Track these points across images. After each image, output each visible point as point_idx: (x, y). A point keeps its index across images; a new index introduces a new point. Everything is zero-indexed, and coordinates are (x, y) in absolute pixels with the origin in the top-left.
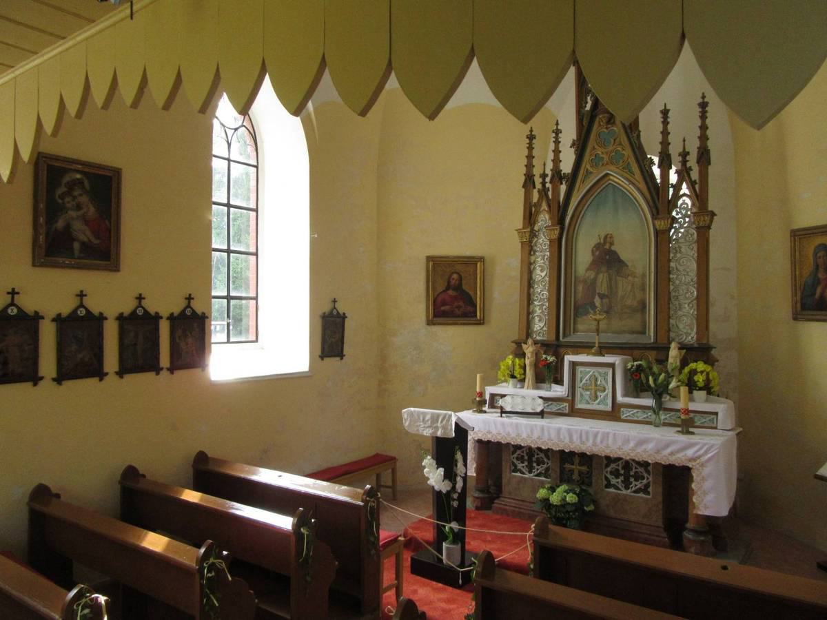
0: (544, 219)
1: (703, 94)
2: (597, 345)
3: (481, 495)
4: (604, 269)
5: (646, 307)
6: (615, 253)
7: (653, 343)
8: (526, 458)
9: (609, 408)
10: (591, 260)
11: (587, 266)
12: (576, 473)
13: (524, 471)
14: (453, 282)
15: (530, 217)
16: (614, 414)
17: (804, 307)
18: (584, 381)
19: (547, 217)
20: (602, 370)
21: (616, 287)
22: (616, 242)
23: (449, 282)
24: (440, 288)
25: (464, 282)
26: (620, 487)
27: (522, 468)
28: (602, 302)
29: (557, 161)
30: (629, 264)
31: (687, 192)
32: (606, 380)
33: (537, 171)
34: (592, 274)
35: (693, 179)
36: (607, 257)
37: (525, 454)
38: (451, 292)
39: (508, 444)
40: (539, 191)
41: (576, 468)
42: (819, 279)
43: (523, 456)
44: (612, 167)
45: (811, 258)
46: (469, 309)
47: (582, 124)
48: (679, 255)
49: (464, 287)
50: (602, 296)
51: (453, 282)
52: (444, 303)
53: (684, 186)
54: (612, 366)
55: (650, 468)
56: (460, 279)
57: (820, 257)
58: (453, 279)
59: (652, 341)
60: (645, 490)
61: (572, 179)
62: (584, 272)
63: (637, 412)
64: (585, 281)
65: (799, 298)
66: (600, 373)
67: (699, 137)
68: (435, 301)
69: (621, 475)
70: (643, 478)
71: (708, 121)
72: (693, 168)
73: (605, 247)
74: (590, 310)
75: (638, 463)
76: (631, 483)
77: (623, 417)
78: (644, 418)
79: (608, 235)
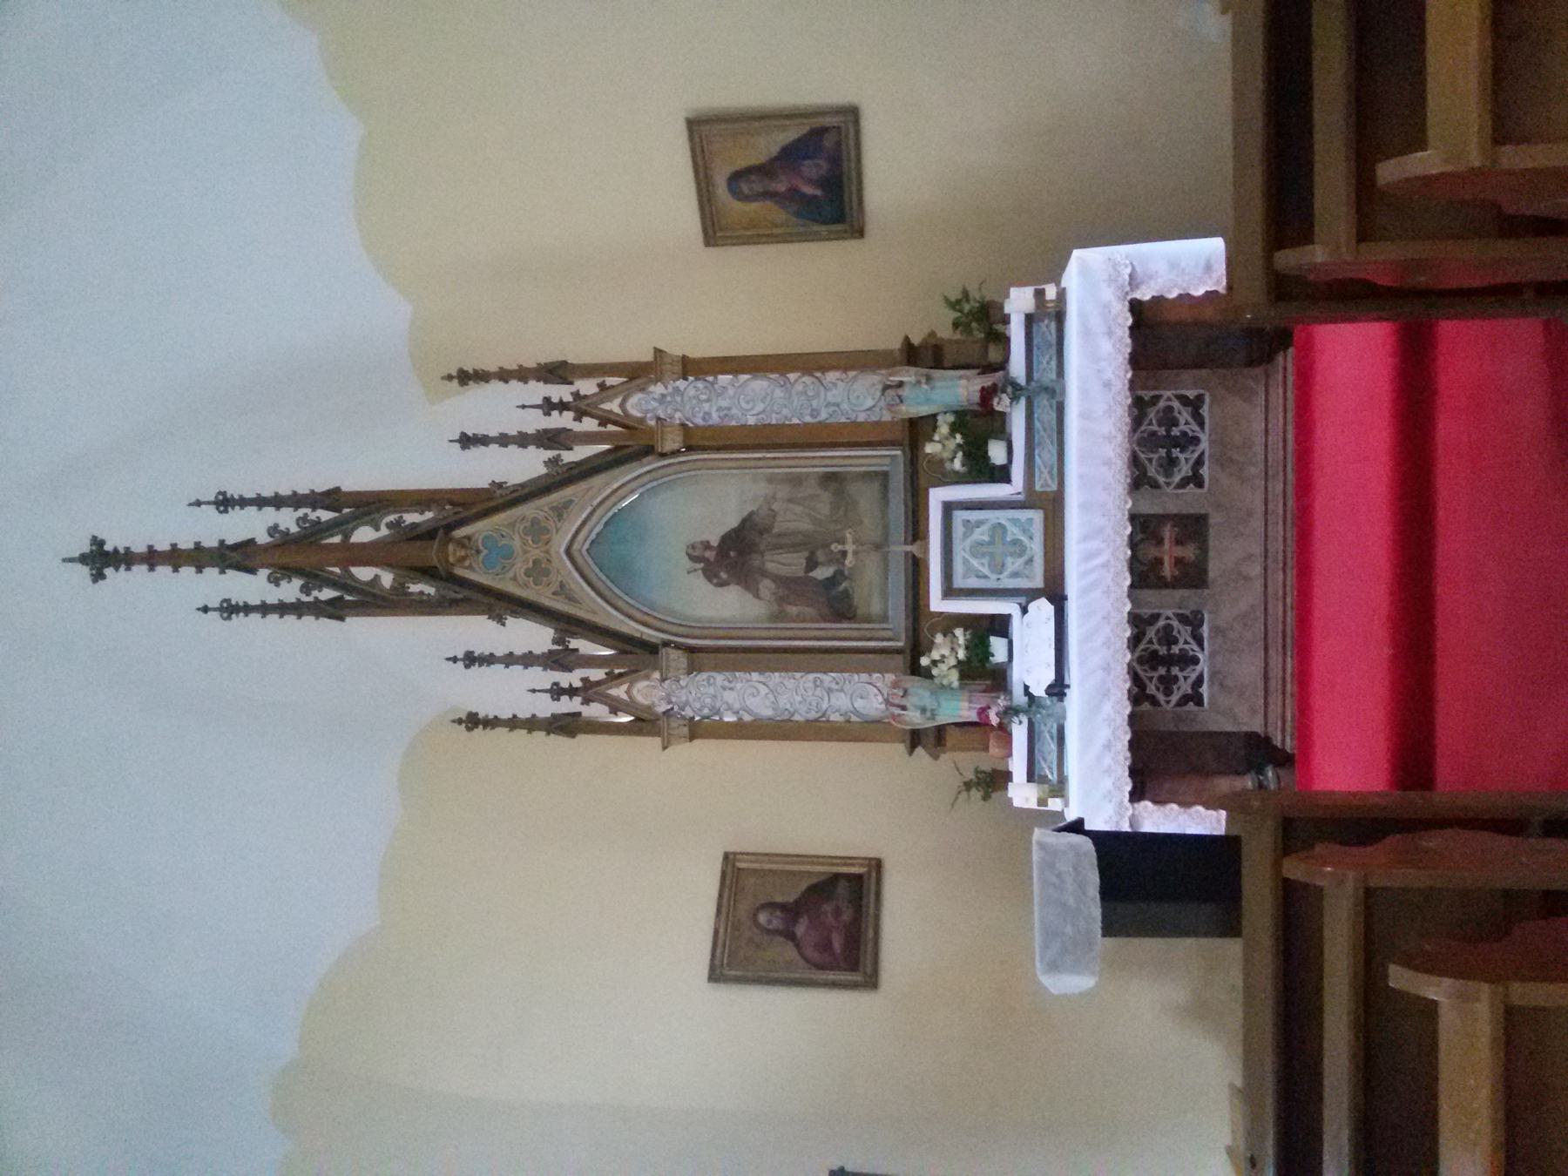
0: (647, 691)
1: (443, 378)
2: (909, 548)
3: (1357, 1115)
4: (756, 561)
5: (833, 474)
6: (726, 539)
7: (903, 451)
8: (1162, 671)
9: (1036, 516)
10: (737, 587)
11: (749, 596)
12: (1179, 551)
13: (1194, 676)
14: (777, 923)
15: (645, 723)
16: (1052, 506)
17: (840, 218)
18: (986, 571)
19: (641, 685)
20: (958, 530)
21: (793, 533)
22: (704, 537)
23: (777, 932)
24: (790, 952)
25: (779, 899)
26: (1196, 455)
27: (1190, 681)
28: (823, 564)
29: (528, 660)
30: (749, 508)
31: (618, 401)
32: (979, 524)
33: (546, 707)
34: (766, 586)
35: (605, 676)
36: (732, 554)
37: (1156, 675)
38: (801, 929)
39: (1133, 719)
40: (586, 701)
41: (1169, 552)
42: (789, 190)
43: (1161, 679)
44: (556, 538)
45: (753, 206)
46: (842, 888)
47: (462, 600)
48: (734, 411)
49: (791, 898)
50: (812, 564)
51: (777, 923)
52: (826, 946)
53: (614, 692)
54: (949, 508)
55: (1147, 395)
56: (771, 906)
57: (751, 189)
58: (770, 922)
59: (899, 453)
60: (1195, 405)
61: (567, 624)
62: (762, 602)
63: (1040, 456)
64: (781, 600)
65: (823, 229)
66: (966, 536)
67: (526, 668)
68: (820, 967)
69: (1169, 453)
70: (1170, 409)
71: (493, 433)
72: (577, 423)
73: (712, 559)
74: (841, 588)
75: (1137, 422)
76: (1184, 434)
77: (1054, 487)
78: (1052, 443)
79: (688, 554)
